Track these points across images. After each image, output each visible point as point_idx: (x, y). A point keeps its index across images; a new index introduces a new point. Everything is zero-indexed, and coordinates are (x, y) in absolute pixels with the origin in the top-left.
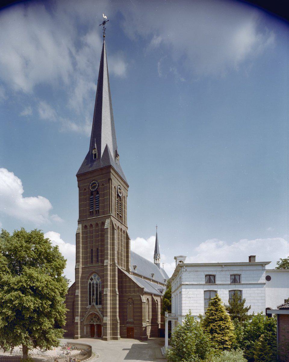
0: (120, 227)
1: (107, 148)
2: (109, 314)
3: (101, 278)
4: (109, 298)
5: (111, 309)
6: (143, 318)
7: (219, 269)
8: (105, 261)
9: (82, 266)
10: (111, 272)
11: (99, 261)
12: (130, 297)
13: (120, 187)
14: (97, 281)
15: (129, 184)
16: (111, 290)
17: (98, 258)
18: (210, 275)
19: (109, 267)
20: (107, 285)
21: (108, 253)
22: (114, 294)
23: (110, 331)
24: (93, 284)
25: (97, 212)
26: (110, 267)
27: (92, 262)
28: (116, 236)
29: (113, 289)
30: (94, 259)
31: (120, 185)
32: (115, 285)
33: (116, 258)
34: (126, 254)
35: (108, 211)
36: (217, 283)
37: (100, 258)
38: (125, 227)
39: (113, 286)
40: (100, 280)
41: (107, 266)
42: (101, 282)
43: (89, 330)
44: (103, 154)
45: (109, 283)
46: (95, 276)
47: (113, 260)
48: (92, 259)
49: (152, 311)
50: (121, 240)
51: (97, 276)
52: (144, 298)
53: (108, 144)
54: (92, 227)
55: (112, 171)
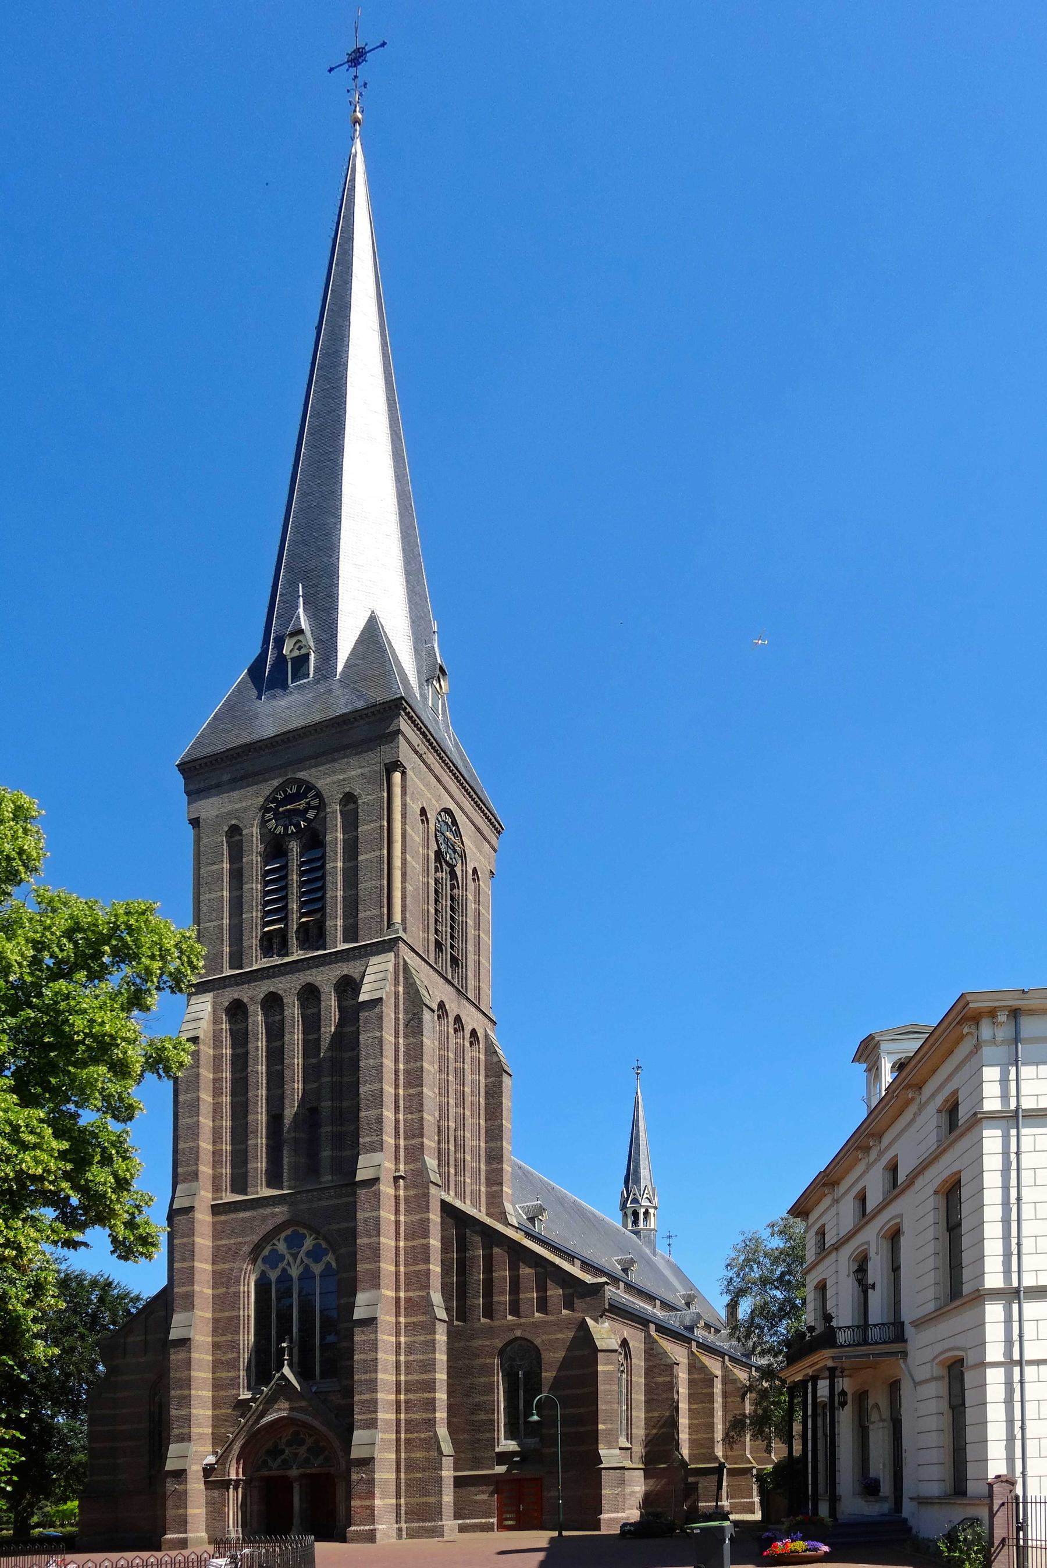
2: (386, 1415)
6: (600, 1427)
9: (214, 1199)
10: (397, 1212)
16: (398, 1300)
21: (380, 1120)
26: (391, 1191)
28: (429, 1042)
33: (430, 1094)
34: (486, 1142)
35: (382, 921)
37: (326, 1154)
38: (481, 1016)
39: (419, 1280)
40: (330, 1258)
41: (377, 1180)
42: (334, 1265)
43: (255, 1508)
44: (353, 652)
47: (415, 1153)
49: (647, 1402)
50: (460, 1073)
51: (308, 1243)
53: (378, 613)
55: (404, 725)
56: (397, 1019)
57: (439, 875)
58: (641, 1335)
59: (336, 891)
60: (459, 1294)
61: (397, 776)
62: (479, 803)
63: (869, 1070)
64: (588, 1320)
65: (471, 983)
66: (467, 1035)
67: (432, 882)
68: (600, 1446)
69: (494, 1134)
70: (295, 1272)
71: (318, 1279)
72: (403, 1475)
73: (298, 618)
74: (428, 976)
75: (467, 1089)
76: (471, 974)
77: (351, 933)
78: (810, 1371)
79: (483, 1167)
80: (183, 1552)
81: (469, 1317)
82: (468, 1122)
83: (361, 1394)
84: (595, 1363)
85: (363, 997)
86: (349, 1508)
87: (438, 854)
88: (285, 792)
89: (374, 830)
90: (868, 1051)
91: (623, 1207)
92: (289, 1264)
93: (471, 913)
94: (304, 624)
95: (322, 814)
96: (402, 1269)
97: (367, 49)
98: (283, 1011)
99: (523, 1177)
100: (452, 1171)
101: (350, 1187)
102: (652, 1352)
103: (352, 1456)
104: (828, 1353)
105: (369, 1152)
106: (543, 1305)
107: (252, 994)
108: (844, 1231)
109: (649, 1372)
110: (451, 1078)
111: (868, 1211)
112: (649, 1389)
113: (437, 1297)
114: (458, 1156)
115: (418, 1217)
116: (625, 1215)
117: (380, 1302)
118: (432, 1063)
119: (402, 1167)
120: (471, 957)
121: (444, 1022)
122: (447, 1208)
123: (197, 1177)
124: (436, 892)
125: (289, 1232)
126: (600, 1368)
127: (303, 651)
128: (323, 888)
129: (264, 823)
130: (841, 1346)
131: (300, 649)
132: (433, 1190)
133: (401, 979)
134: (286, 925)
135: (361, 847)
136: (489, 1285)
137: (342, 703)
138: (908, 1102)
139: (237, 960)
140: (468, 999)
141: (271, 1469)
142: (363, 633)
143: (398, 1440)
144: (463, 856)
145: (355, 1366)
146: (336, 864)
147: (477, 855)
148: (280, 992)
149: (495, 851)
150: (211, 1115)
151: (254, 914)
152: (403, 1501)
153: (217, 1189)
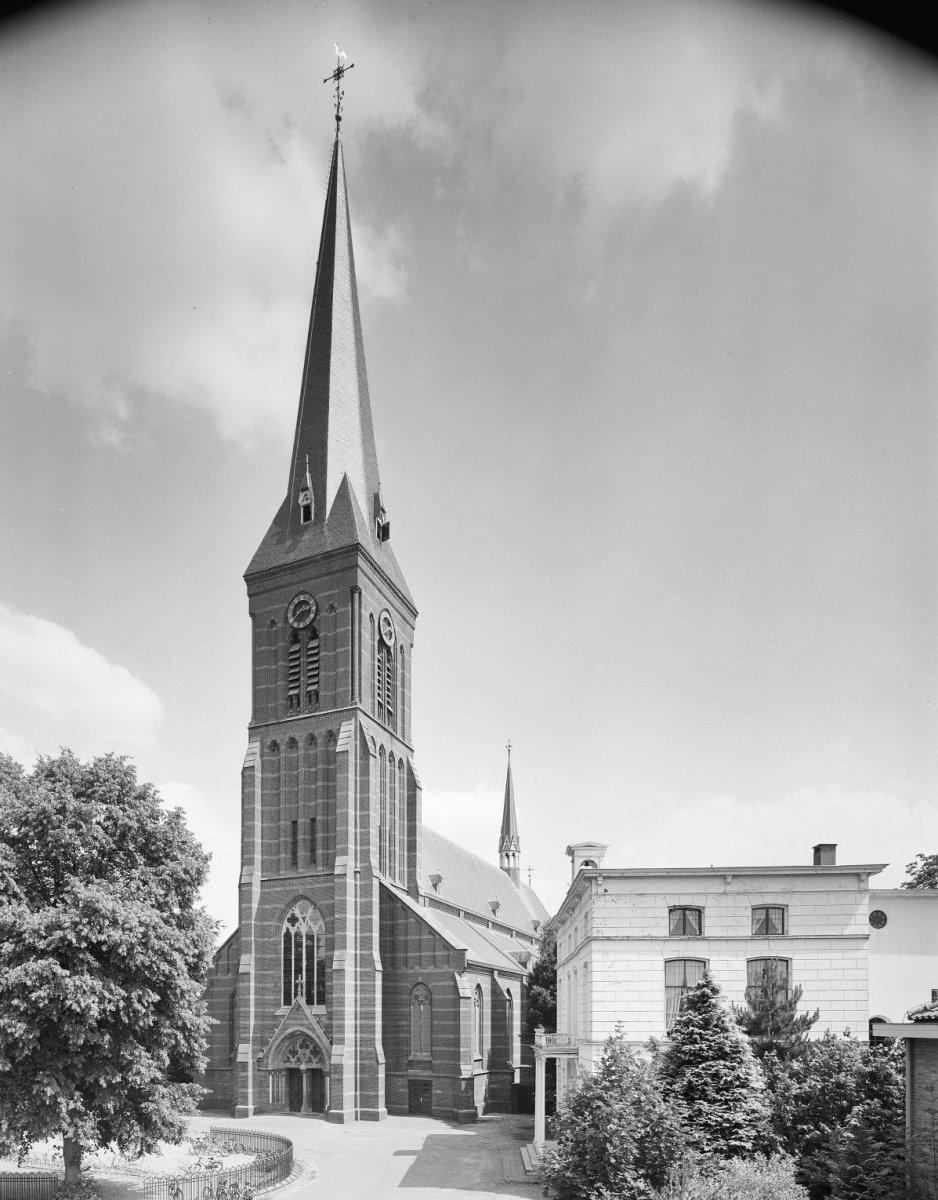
7: (716, 886)
8: (339, 861)
11: (319, 858)
12: (420, 979)
13: (388, 616)
15: (418, 606)
17: (313, 850)
18: (684, 909)
19: (350, 881)
21: (344, 903)
25: (314, 698)
30: (302, 853)
31: (387, 610)
36: (708, 932)
38: (405, 748)
39: (365, 943)
47: (365, 855)
48: (294, 853)
52: (466, 983)
53: (349, 475)
54: (295, 748)
55: (361, 561)
58: (489, 979)
91: (501, 851)
93: (399, 678)
94: (309, 484)
97: (345, 68)
102: (495, 990)
109: (494, 1007)
112: (493, 1019)
113: (376, 955)
152: (358, 1093)
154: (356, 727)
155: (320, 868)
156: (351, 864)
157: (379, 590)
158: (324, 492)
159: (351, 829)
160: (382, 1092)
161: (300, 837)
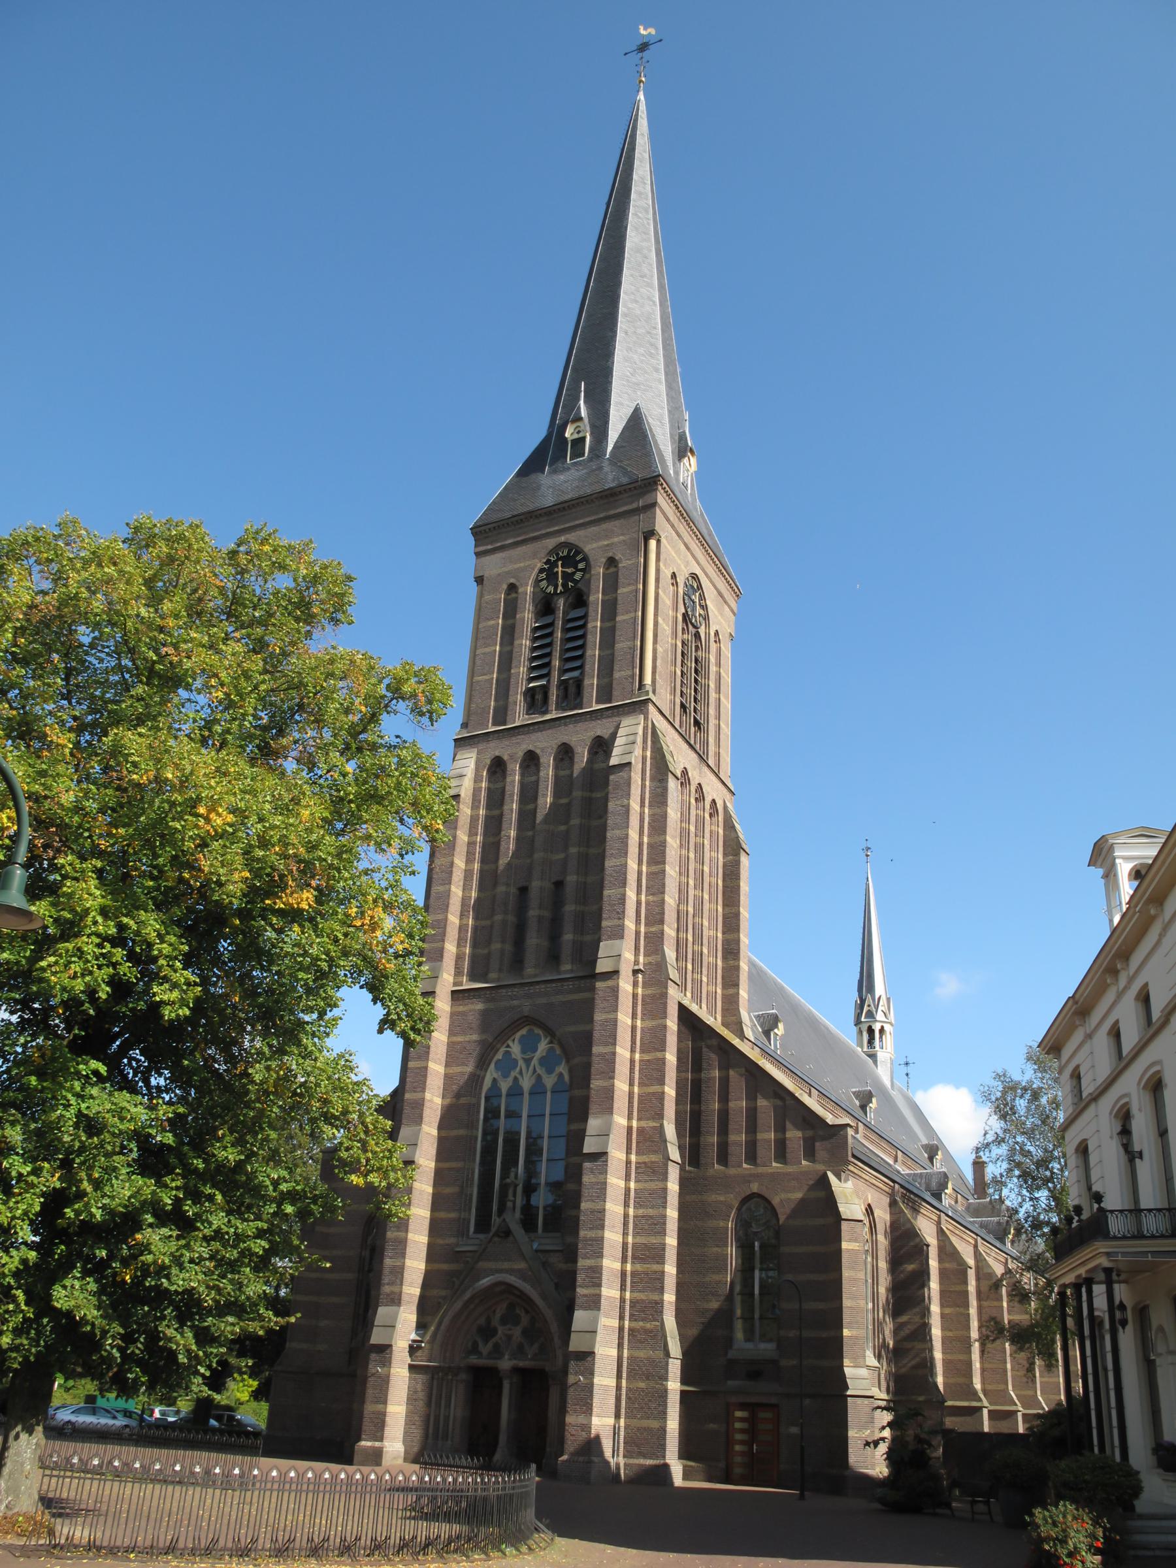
0: (695, 776)
1: (636, 422)
2: (610, 1292)
3: (567, 1055)
4: (615, 1182)
5: (624, 1260)
6: (846, 1332)
8: (605, 948)
9: (455, 984)
11: (566, 951)
12: (755, 1187)
14: (539, 1077)
17: (554, 937)
19: (625, 985)
20: (609, 1093)
21: (623, 899)
22: (654, 1158)
23: (611, 1421)
24: (515, 1092)
27: (517, 962)
29: (644, 1124)
30: (534, 941)
32: (661, 1096)
34: (724, 933)
37: (568, 937)
39: (650, 1106)
40: (562, 1068)
41: (616, 973)
42: (567, 1077)
45: (621, 1086)
46: (529, 1046)
47: (655, 942)
50: (699, 848)
51: (543, 1046)
52: (854, 1195)
54: (533, 768)
55: (661, 499)
56: (643, 786)
57: (686, 636)
59: (594, 652)
60: (692, 1125)
61: (653, 543)
62: (722, 569)
63: (1106, 876)
64: (830, 1174)
65: (712, 749)
66: (707, 806)
67: (679, 644)
68: (846, 1362)
69: (731, 924)
70: (526, 1083)
71: (526, 1096)
72: (624, 1383)
73: (579, 408)
74: (673, 740)
75: (706, 869)
76: (711, 740)
77: (605, 693)
78: (1082, 1271)
79: (720, 963)
80: (377, 1469)
81: (703, 1161)
82: (706, 906)
83: (585, 1257)
84: (838, 1239)
85: (614, 761)
86: (562, 1424)
87: (685, 616)
88: (557, 554)
89: (631, 592)
90: (1102, 854)
91: (858, 1022)
92: (521, 1073)
93: (712, 676)
95: (587, 576)
96: (636, 1089)
98: (538, 771)
99: (757, 975)
100: (690, 967)
101: (589, 977)
103: (572, 1348)
104: (1101, 1246)
105: (610, 938)
106: (781, 1153)
107: (513, 751)
108: (1100, 1079)
110: (692, 855)
111: (1125, 1053)
114: (696, 948)
115: (654, 1023)
116: (860, 1032)
117: (614, 1132)
118: (673, 837)
119: (641, 959)
120: (713, 722)
121: (701, 805)
122: (685, 1015)
123: (442, 956)
124: (683, 654)
125: (524, 1031)
126: (845, 1245)
127: (581, 435)
128: (583, 647)
129: (537, 582)
130: (1115, 1238)
131: (579, 432)
132: (672, 991)
133: (649, 743)
134: (548, 681)
135: (620, 608)
136: (724, 1116)
137: (610, 478)
138: (1152, 919)
139: (501, 715)
140: (708, 766)
141: (480, 1354)
142: (629, 420)
143: (621, 1329)
144: (706, 618)
145: (582, 1218)
146: (596, 624)
147: (721, 619)
148: (538, 751)
149: (734, 614)
150: (461, 883)
151: (521, 670)
153: (458, 972)
154: (645, 728)
155: (568, 967)
156: (628, 955)
157: (686, 545)
158: (606, 422)
159: (631, 894)
160: (1009, 1374)
161: (533, 913)
